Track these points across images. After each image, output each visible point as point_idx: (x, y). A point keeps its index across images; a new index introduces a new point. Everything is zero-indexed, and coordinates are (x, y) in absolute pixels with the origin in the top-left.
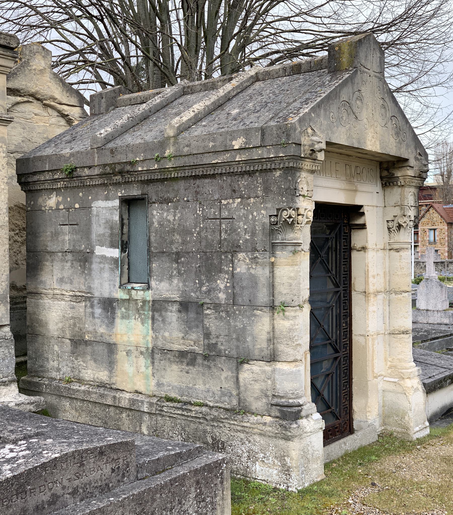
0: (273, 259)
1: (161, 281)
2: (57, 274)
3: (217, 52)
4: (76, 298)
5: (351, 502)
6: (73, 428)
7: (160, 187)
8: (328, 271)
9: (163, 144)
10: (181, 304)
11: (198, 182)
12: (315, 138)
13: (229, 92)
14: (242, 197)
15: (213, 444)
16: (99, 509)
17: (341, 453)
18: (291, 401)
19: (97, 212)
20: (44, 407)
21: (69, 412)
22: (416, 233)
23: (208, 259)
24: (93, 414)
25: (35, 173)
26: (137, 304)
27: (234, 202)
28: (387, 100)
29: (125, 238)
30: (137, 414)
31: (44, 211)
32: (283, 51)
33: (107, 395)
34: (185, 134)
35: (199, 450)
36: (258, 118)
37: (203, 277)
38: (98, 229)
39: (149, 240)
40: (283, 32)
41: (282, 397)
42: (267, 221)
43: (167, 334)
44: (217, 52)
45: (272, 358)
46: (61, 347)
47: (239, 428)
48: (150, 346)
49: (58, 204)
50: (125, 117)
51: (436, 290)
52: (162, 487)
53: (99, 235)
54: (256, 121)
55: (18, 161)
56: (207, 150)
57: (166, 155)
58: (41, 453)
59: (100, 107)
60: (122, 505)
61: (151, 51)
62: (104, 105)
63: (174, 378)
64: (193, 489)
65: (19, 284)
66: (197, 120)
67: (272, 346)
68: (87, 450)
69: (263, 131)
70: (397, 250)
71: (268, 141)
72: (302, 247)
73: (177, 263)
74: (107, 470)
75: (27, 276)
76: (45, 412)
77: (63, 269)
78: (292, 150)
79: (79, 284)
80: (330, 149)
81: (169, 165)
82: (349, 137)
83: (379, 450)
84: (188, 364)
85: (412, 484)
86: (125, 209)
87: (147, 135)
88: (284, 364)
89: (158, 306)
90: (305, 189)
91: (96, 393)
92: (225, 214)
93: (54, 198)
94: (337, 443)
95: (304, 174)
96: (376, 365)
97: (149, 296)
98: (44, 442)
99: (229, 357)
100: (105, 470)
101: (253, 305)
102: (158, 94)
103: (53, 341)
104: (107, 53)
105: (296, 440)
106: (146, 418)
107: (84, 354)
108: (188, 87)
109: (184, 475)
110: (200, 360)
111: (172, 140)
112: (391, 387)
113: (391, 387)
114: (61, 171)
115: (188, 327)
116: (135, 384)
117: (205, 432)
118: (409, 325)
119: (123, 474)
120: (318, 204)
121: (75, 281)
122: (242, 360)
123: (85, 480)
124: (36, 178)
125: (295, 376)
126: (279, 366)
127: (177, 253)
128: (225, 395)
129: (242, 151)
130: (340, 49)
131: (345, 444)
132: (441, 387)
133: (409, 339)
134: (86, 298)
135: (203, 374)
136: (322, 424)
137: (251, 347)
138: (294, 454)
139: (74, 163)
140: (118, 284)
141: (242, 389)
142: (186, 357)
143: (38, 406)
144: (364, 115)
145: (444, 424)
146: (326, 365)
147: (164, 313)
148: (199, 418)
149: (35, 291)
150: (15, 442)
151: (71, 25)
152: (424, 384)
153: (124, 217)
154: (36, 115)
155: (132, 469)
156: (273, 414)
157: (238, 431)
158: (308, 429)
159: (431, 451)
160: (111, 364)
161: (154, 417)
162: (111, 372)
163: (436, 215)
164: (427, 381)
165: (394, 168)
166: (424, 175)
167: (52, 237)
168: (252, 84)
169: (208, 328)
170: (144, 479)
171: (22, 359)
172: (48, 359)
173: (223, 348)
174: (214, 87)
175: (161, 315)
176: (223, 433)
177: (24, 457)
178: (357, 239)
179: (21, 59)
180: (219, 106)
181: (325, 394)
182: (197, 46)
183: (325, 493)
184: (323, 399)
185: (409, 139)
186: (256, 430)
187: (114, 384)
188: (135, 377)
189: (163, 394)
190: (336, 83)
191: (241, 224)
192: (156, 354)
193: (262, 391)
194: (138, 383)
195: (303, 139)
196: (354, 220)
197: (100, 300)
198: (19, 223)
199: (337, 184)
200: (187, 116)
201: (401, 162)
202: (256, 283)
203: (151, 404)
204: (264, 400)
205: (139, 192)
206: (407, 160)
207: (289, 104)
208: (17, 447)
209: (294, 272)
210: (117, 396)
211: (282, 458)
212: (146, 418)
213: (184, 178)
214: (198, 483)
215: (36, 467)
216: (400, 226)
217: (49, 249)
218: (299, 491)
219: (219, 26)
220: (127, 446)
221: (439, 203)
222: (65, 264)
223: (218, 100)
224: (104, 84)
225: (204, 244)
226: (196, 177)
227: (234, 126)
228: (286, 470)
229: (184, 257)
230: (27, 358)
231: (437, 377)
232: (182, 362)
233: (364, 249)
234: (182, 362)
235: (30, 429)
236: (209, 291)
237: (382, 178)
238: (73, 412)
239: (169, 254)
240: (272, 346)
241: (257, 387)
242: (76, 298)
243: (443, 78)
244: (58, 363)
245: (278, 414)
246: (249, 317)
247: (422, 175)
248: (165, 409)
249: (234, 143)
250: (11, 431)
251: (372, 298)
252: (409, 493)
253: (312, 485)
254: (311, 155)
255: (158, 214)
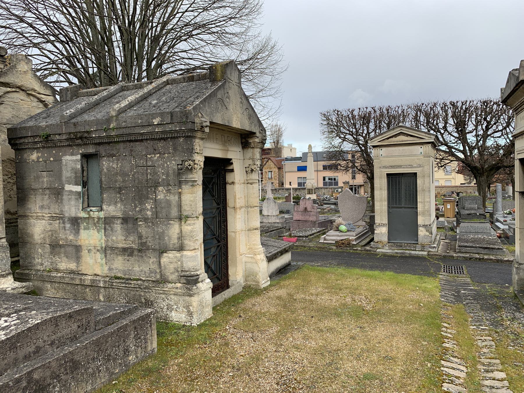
0: (180, 190)
1: (109, 205)
2: (39, 203)
3: (144, 68)
4: (53, 218)
5: (227, 328)
6: (51, 302)
7: (107, 147)
8: (213, 196)
9: (109, 120)
10: (123, 219)
11: (132, 144)
12: (203, 119)
13: (151, 90)
14: (160, 153)
15: (145, 303)
16: (70, 352)
17: (222, 300)
18: (192, 273)
19: (66, 163)
20: (32, 289)
21: (50, 291)
22: (262, 174)
23: (139, 191)
24: (67, 291)
25: (21, 138)
26: (94, 220)
27: (155, 157)
28: (243, 99)
29: (85, 179)
30: (96, 288)
31: (29, 163)
32: (184, 69)
33: (75, 278)
34: (123, 115)
35: (136, 308)
36: (169, 106)
37: (137, 202)
38: (67, 174)
39: (101, 180)
40: (184, 58)
41: (187, 271)
42: (175, 167)
43: (114, 238)
44: (144, 68)
45: (181, 248)
46: (43, 250)
47: (161, 292)
48: (104, 246)
49: (38, 158)
50: (83, 103)
51: (272, 204)
52: (112, 333)
53: (68, 178)
54: (167, 108)
55: (8, 130)
56: (137, 124)
57: (111, 127)
58: (28, 321)
59: (67, 96)
60: (86, 347)
61: (102, 64)
62: (69, 96)
63: (119, 264)
64: (132, 332)
65: (12, 210)
66: (130, 106)
67: (180, 242)
68: (60, 316)
69: (172, 114)
70: (251, 184)
71: (175, 120)
72: (197, 182)
73: (120, 194)
74: (75, 326)
75: (18, 205)
76: (33, 293)
77: (43, 199)
78: (190, 126)
79: (55, 209)
80: (212, 126)
81: (113, 134)
82: (223, 119)
83: (243, 296)
84: (128, 256)
85: (261, 313)
86: (85, 161)
87: (98, 114)
88: (188, 251)
89: (108, 221)
90: (198, 149)
91: (68, 277)
92: (150, 163)
93: (36, 154)
94: (220, 294)
95: (197, 140)
96: (241, 248)
97: (102, 214)
98: (29, 314)
99: (154, 250)
100: (73, 327)
101: (168, 218)
102: (105, 90)
103: (37, 246)
104: (73, 65)
105: (196, 296)
106: (102, 290)
107: (59, 254)
108: (125, 86)
109: (127, 324)
110: (136, 253)
111: (114, 118)
112: (250, 260)
113: (250, 260)
114: (40, 137)
115: (128, 233)
116: (94, 270)
117: (140, 296)
118: (258, 225)
119: (86, 328)
120: (206, 158)
121: (51, 207)
122: (162, 251)
123: (59, 335)
124: (22, 141)
125: (195, 258)
126: (185, 253)
127: (120, 188)
128: (152, 273)
129: (159, 126)
130: (216, 68)
131: (224, 295)
132: (276, 258)
133: (258, 233)
134: (60, 218)
135: (138, 261)
136: (211, 285)
137: (168, 243)
138: (195, 304)
139: (48, 131)
140: (81, 208)
141: (163, 268)
142: (127, 252)
143: (28, 289)
144: (231, 107)
145: (278, 278)
146: (213, 250)
147: (112, 225)
148: (136, 288)
149: (23, 214)
150: (8, 315)
151: (49, 46)
152: (267, 257)
153: (84, 166)
154: (22, 100)
155: (92, 324)
156: (182, 282)
157: (161, 293)
158: (203, 289)
159: (271, 294)
160: (78, 258)
161: (107, 290)
162: (78, 263)
163: (272, 163)
164: (268, 255)
165: (249, 138)
166: (264, 141)
167: (35, 179)
168: (165, 86)
169: (140, 233)
170: (100, 329)
171: (16, 259)
172: (34, 258)
173: (150, 244)
174: (141, 87)
175: (110, 226)
176: (151, 296)
177: (15, 325)
178: (229, 178)
179: (10, 64)
180: (144, 98)
181: (213, 267)
182: (131, 63)
183: (213, 325)
184: (212, 270)
185: (256, 122)
186: (172, 292)
187: (80, 271)
188: (94, 265)
189: (113, 275)
190: (214, 88)
191: (160, 169)
192: (107, 250)
193: (175, 268)
194: (96, 269)
195: (196, 120)
196: (227, 167)
197: (69, 219)
198: (11, 171)
200: (124, 103)
201: (251, 134)
202: (170, 205)
203: (105, 282)
204: (176, 274)
205: (94, 151)
206: (255, 133)
207: (187, 99)
208: (10, 319)
209: (193, 198)
210: (83, 278)
211: (187, 307)
212: (102, 290)
213: (123, 141)
214: (135, 328)
215: (24, 331)
216: (252, 170)
217: (33, 187)
218: (198, 325)
219: (145, 53)
220: (88, 311)
221: (274, 157)
222: (45, 196)
223: (144, 95)
224: (70, 83)
225: (137, 182)
226: (131, 141)
227: (154, 111)
228: (190, 314)
229: (124, 190)
230: (19, 258)
231: (273, 253)
232: (125, 254)
233: (233, 183)
234: (125, 254)
235: (19, 306)
236: (141, 211)
237: (242, 143)
238: (53, 290)
239: (114, 188)
240: (180, 242)
241: (172, 266)
242: (53, 218)
243: (273, 92)
244: (41, 260)
245: (185, 282)
246: (166, 225)
247: (263, 142)
248: (114, 284)
249: (154, 121)
250: (6, 308)
251: (238, 211)
252: (260, 319)
253: (205, 321)
254: (201, 129)
255: (105, 164)
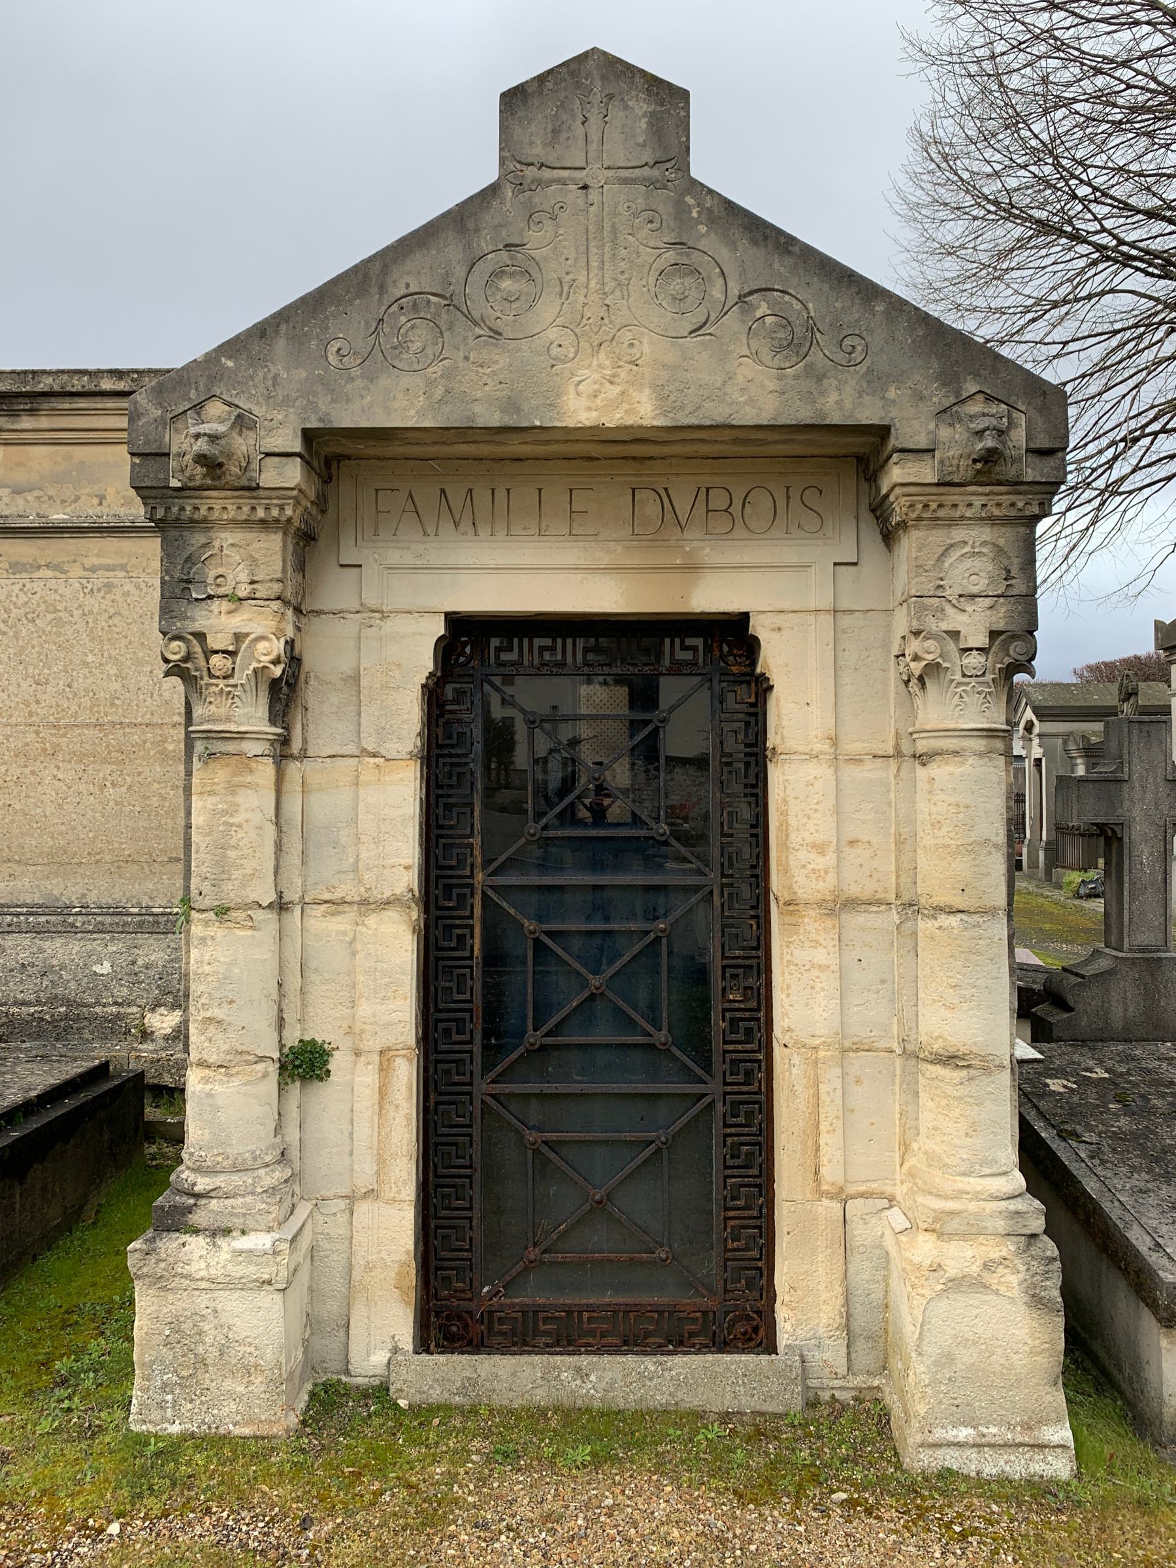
70: (922, 759)
199: (571, 554)
